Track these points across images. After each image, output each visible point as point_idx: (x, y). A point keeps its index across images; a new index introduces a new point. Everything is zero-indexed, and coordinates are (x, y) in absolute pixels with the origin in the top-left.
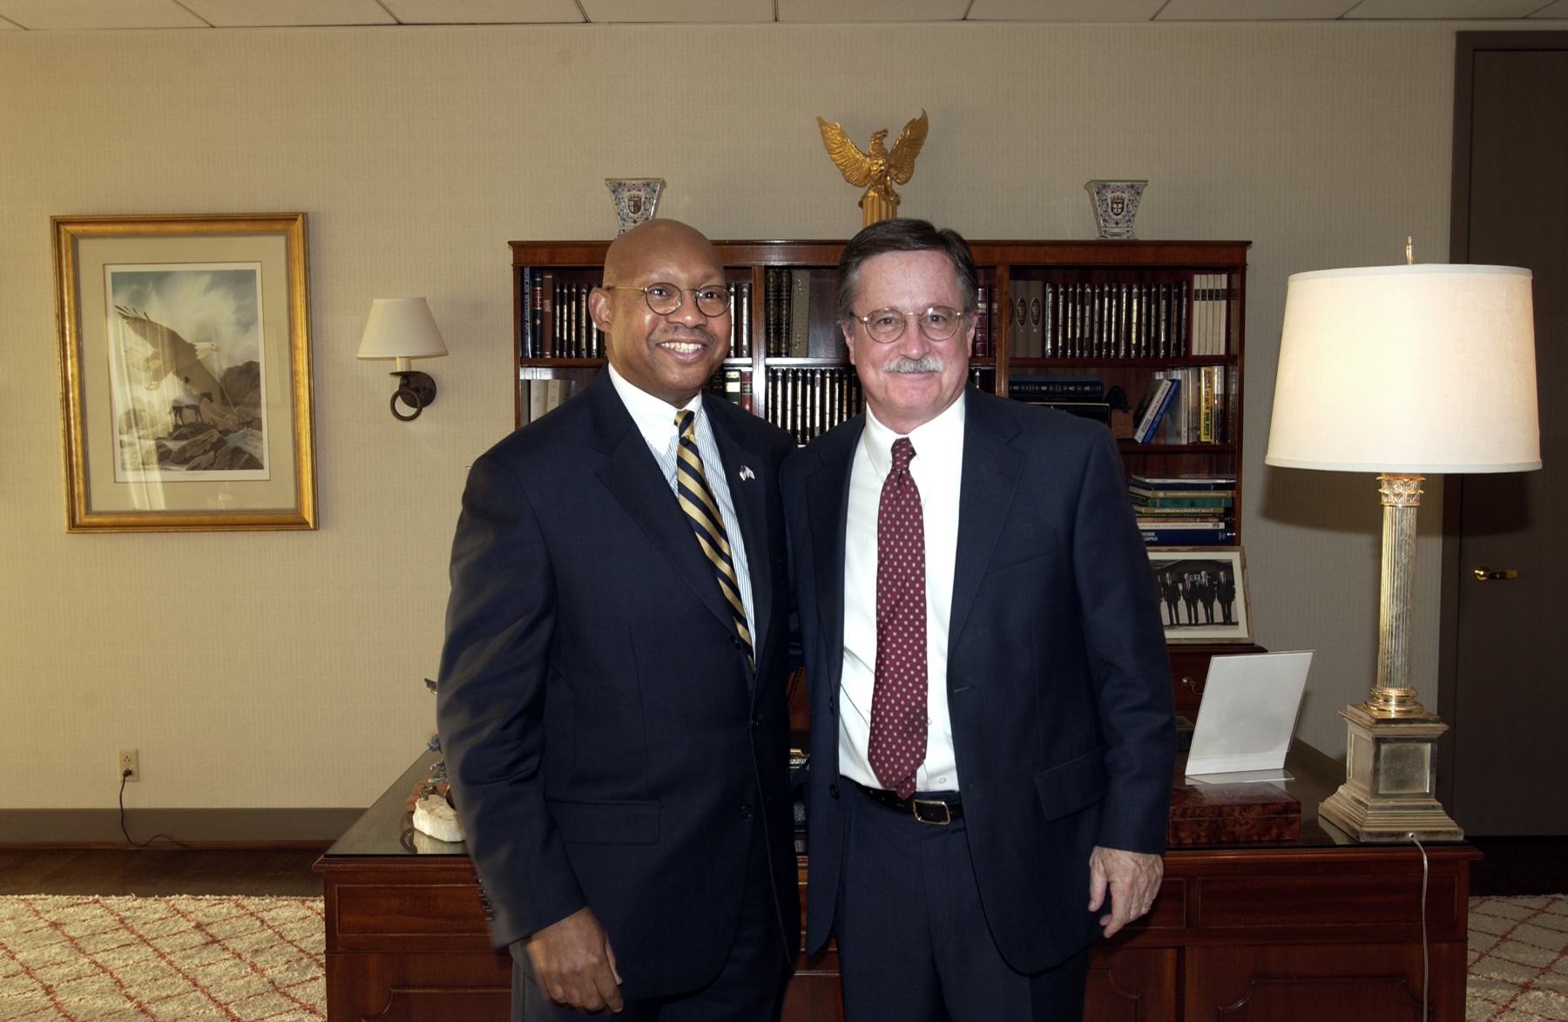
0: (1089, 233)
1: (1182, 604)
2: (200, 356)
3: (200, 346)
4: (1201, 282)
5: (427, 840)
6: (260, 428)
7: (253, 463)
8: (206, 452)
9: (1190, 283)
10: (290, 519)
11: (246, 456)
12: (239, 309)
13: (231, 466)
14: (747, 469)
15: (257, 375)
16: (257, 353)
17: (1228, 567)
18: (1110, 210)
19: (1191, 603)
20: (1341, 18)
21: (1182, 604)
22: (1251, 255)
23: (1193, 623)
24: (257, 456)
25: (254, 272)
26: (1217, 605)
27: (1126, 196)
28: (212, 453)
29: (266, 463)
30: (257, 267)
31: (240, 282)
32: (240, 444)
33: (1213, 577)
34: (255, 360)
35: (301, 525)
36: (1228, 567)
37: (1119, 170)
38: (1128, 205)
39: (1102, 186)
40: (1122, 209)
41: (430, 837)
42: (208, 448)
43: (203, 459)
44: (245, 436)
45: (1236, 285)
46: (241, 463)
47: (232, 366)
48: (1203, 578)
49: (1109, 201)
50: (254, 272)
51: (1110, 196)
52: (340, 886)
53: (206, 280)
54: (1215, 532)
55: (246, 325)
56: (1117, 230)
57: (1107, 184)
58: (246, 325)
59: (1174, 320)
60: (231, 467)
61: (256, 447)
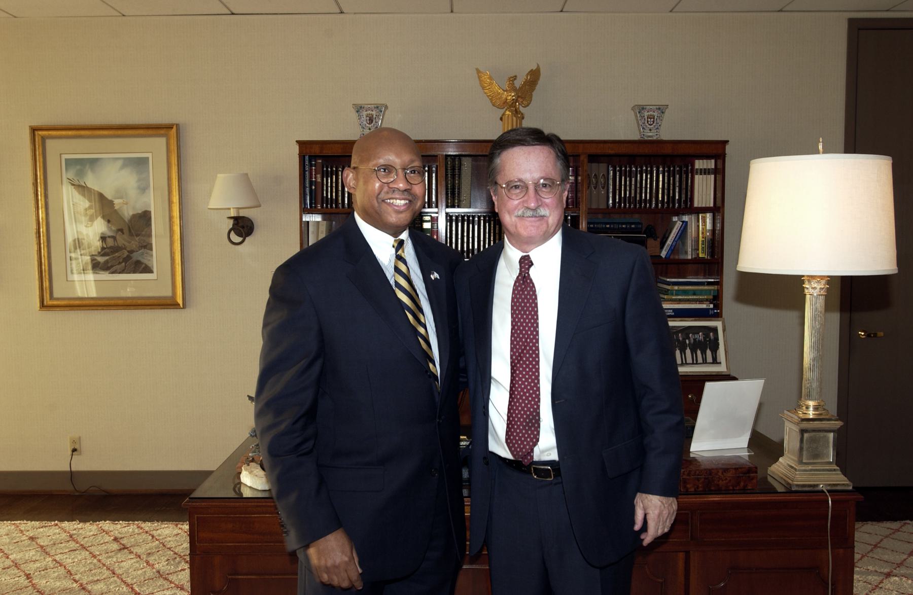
0: (634, 136)
1: (688, 351)
2: (116, 207)
3: (116, 202)
4: (699, 164)
5: (249, 489)
6: (151, 249)
7: (147, 270)
8: (120, 263)
9: (693, 165)
10: (169, 302)
11: (143, 266)
12: (139, 180)
13: (134, 271)
14: (435, 273)
15: (150, 219)
16: (149, 206)
17: (715, 330)
18: (646, 122)
19: (693, 351)
20: (781, 11)
21: (688, 351)
22: (728, 149)
23: (695, 363)
24: (150, 266)
25: (148, 158)
26: (709, 352)
27: (656, 114)
28: (123, 264)
29: (155, 270)
30: (149, 155)
31: (140, 164)
32: (140, 259)
33: (706, 336)
34: (148, 210)
35: (175, 305)
36: (715, 330)
37: (651, 99)
38: (657, 119)
39: (641, 108)
40: (654, 122)
41: (250, 487)
42: (121, 261)
43: (118, 267)
44: (143, 254)
45: (720, 166)
46: (140, 269)
47: (135, 213)
48: (700, 336)
49: (646, 117)
50: (148, 158)
51: (646, 114)
52: (198, 516)
53: (120, 163)
54: (707, 310)
55: (143, 189)
56: (650, 134)
57: (645, 107)
58: (143, 189)
59: (684, 186)
60: (134, 272)
61: (149, 260)
